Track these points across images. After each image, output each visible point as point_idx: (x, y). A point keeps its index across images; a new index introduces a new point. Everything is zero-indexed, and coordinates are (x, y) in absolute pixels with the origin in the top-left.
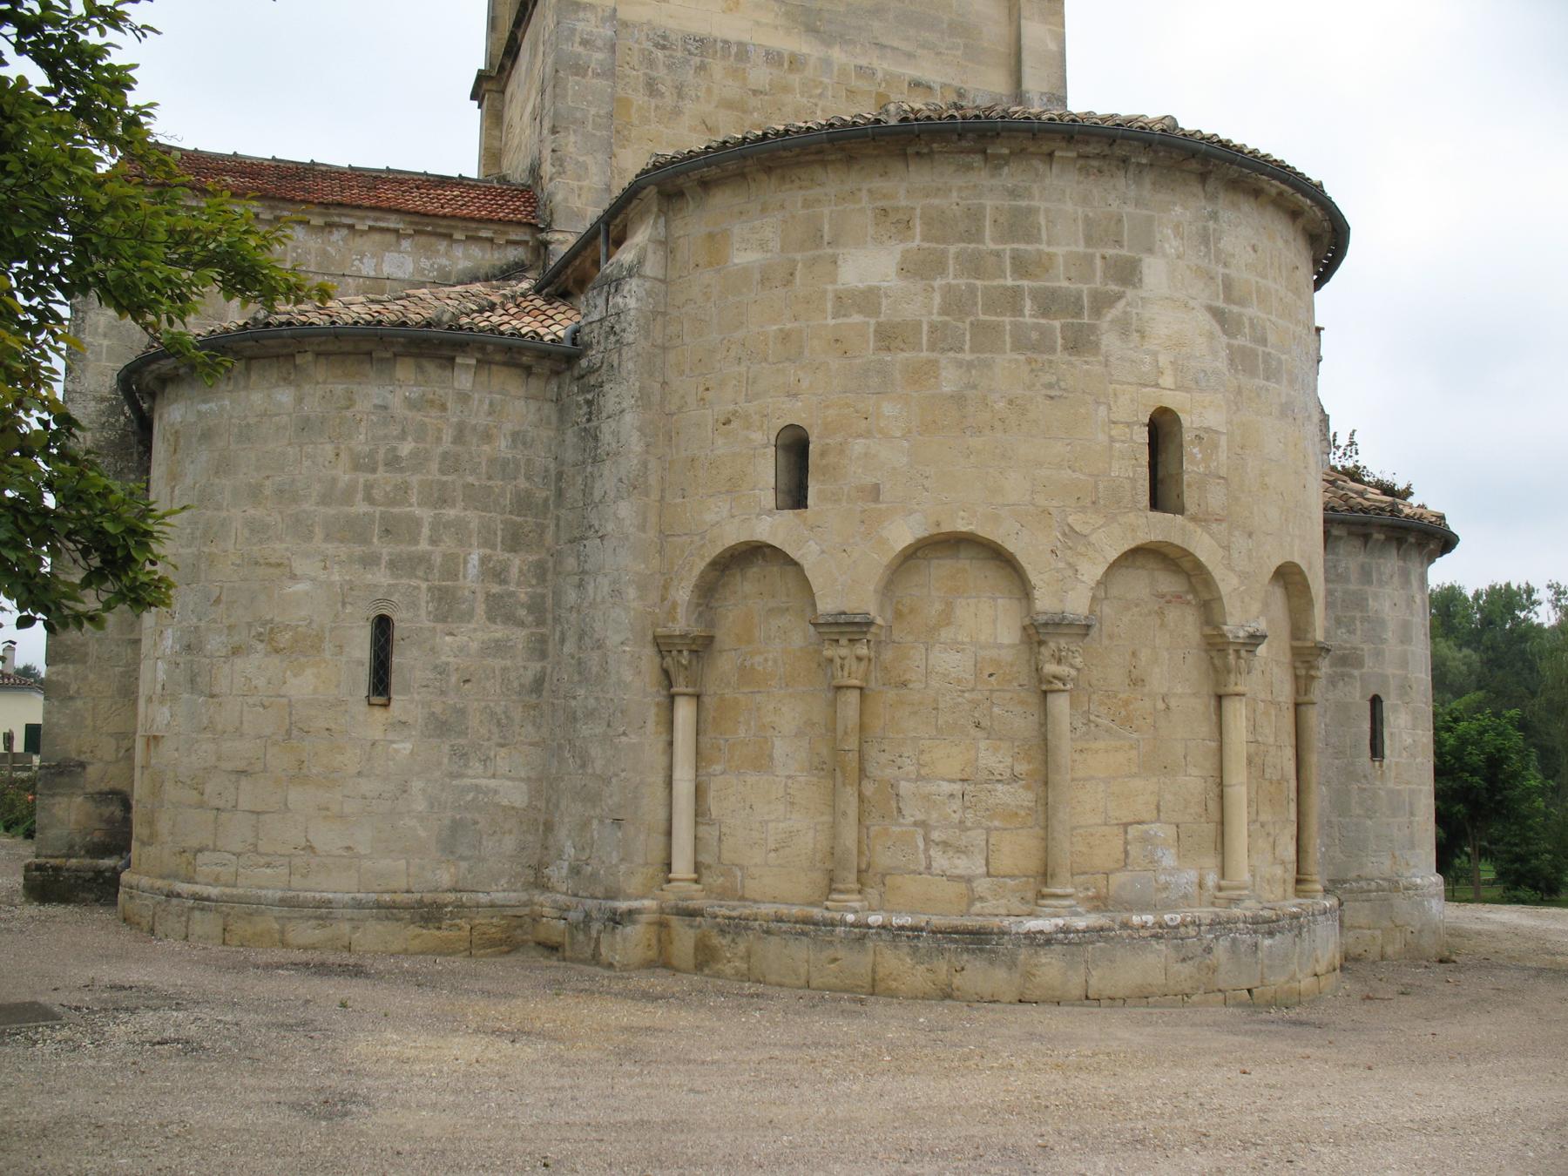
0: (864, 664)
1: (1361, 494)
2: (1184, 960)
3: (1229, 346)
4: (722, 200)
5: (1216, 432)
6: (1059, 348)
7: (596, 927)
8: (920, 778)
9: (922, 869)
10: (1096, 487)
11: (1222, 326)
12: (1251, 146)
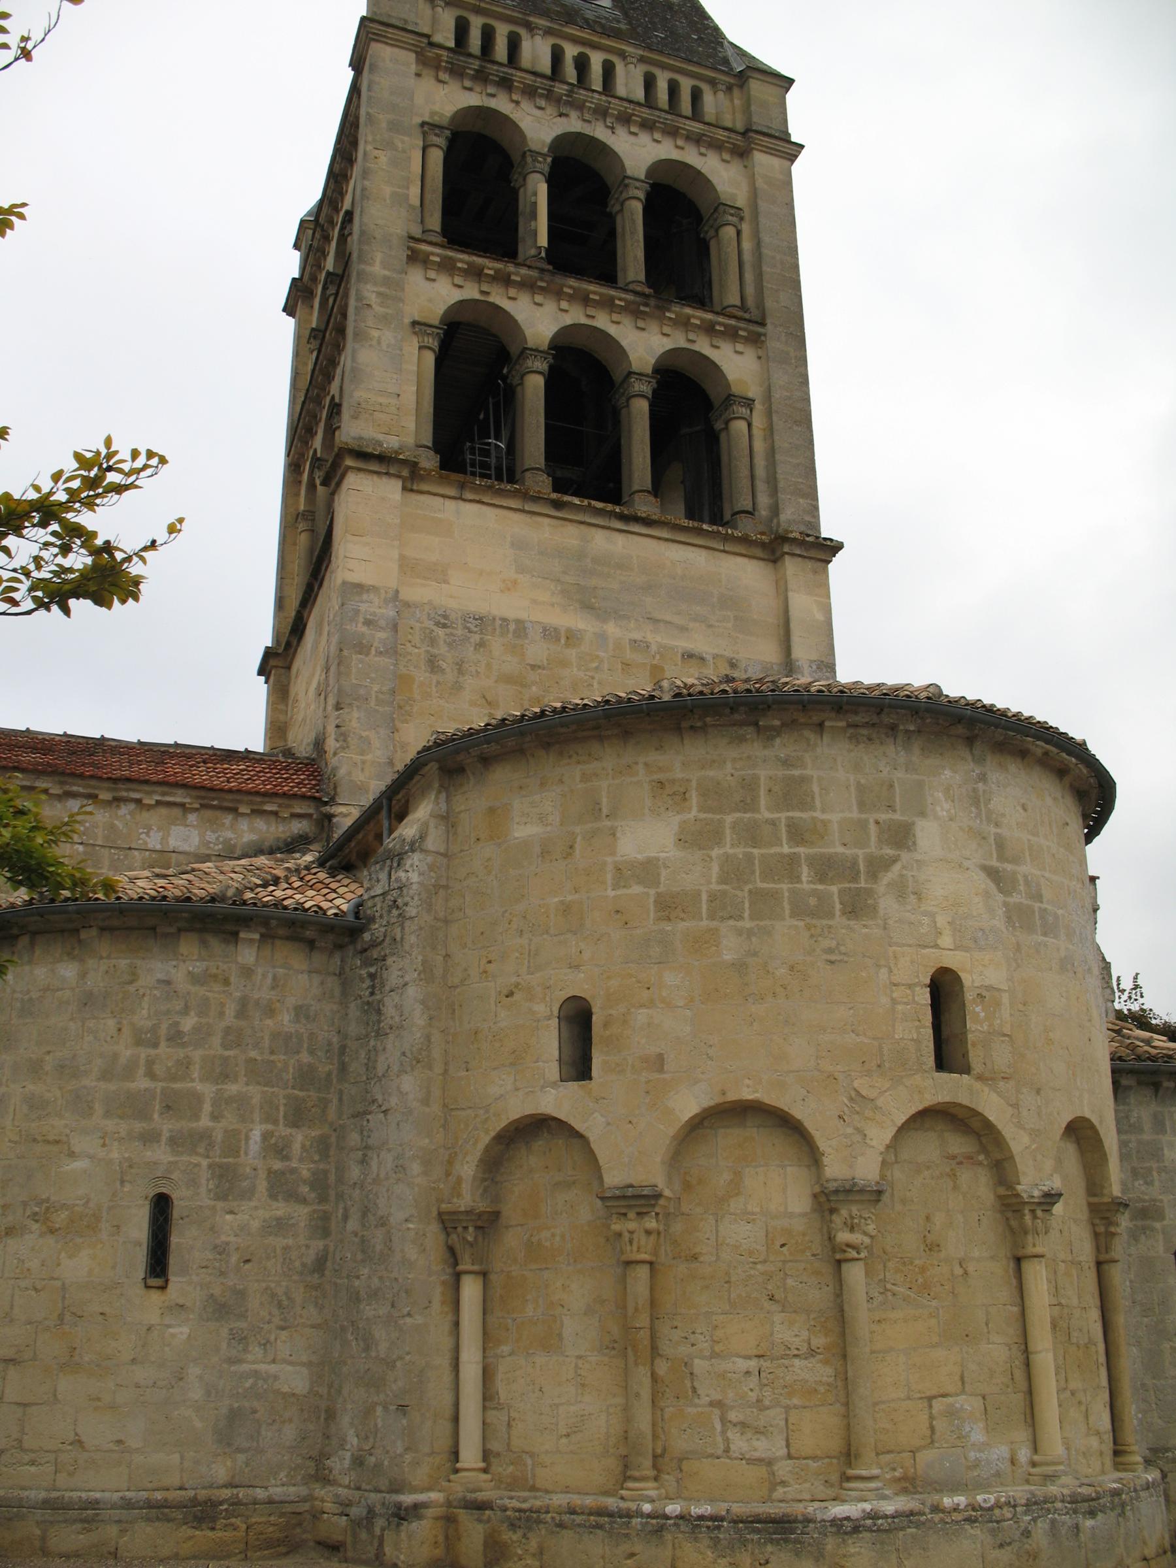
0: (653, 1238)
1: (1148, 1042)
2: (1001, 1546)
3: (1005, 904)
4: (501, 774)
5: (999, 990)
6: (838, 913)
7: (380, 1523)
8: (714, 1355)
9: (719, 1452)
10: (880, 1048)
11: (998, 885)
12: (1014, 710)
